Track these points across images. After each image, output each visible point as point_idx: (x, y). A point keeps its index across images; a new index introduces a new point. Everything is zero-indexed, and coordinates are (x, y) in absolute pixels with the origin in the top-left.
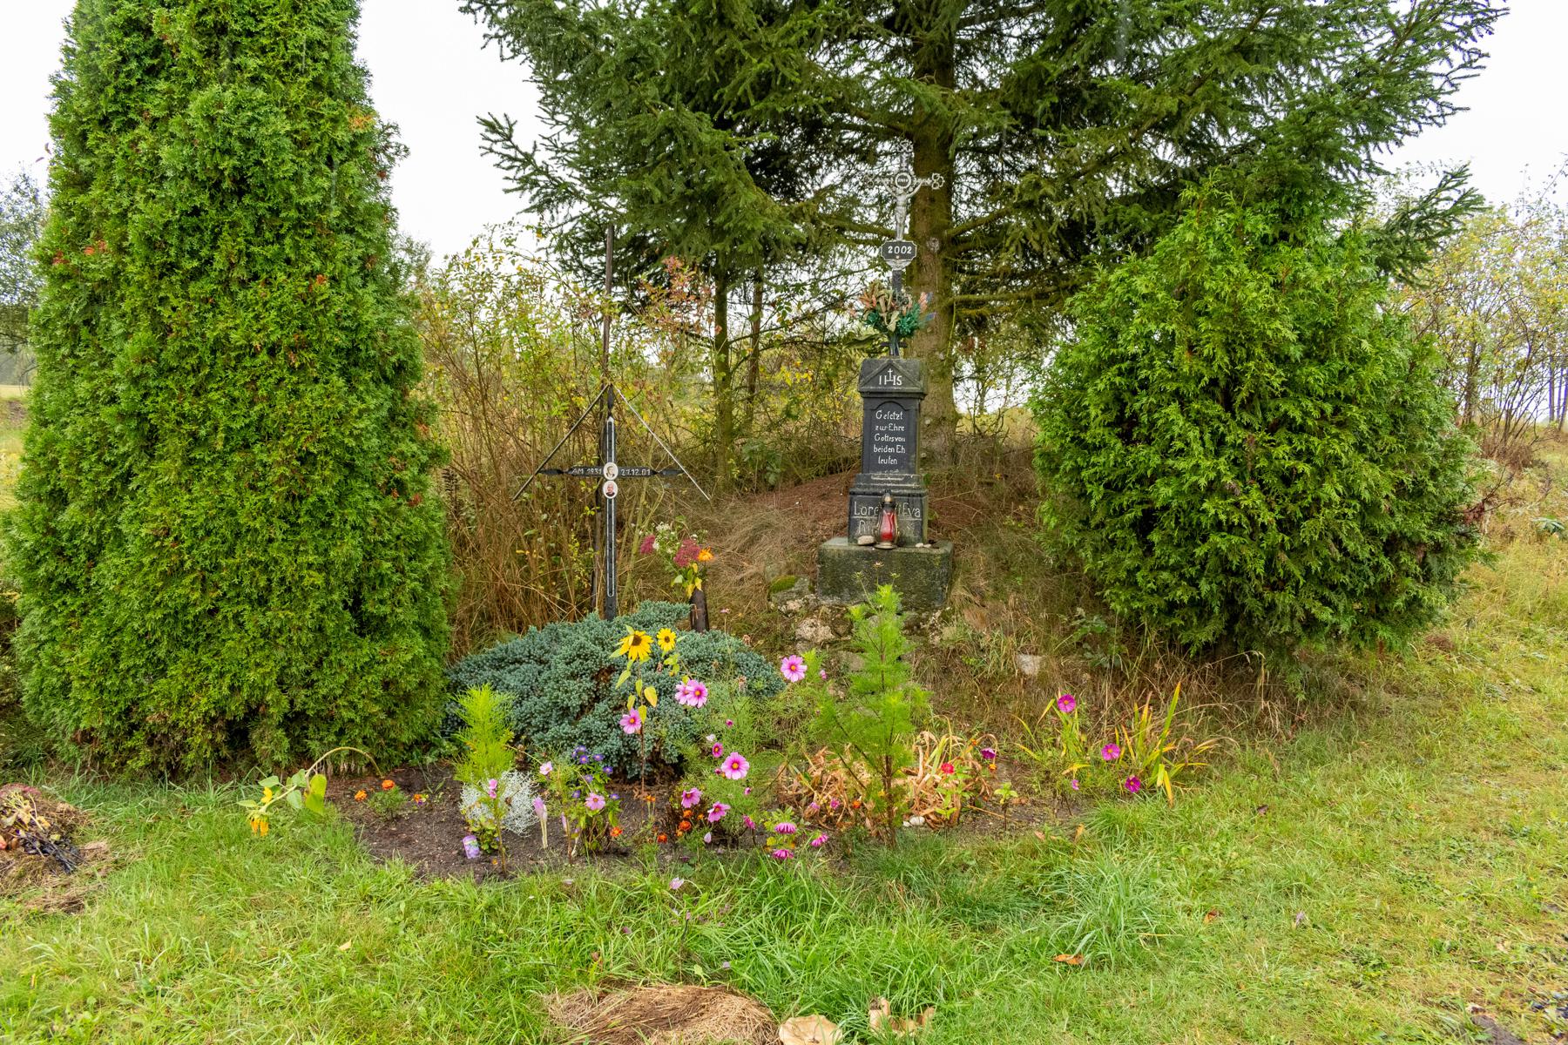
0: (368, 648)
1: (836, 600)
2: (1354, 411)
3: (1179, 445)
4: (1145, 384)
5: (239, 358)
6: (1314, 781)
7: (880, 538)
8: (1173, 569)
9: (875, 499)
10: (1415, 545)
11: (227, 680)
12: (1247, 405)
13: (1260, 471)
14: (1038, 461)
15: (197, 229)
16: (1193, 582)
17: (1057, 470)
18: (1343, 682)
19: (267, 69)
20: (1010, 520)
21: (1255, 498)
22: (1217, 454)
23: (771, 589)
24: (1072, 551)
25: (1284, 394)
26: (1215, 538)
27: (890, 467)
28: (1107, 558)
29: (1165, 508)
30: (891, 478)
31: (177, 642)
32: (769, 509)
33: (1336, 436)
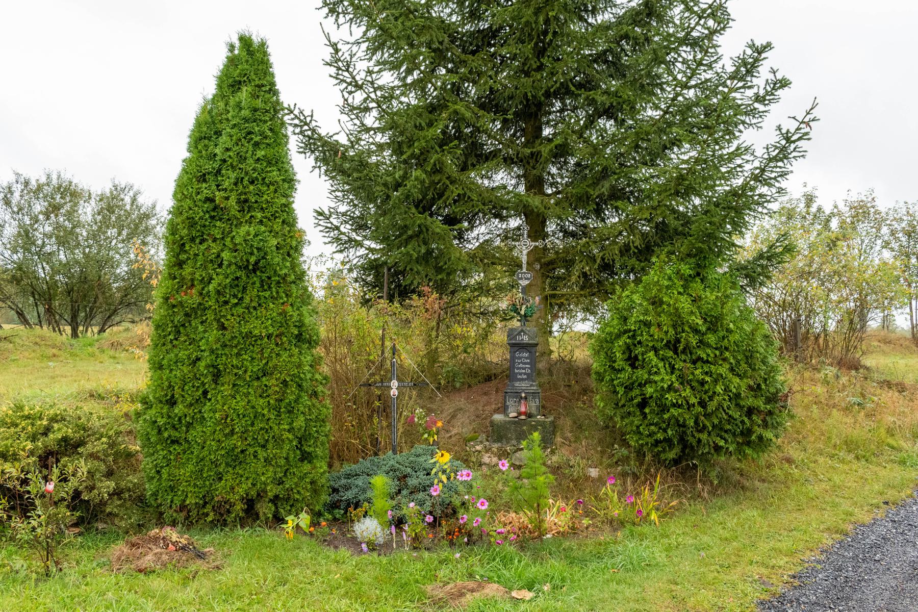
0: (306, 467)
1: (500, 444)
2: (727, 354)
3: (655, 370)
4: (640, 343)
5: (256, 341)
6: (719, 516)
7: (520, 414)
8: (656, 425)
9: (517, 395)
10: (760, 412)
11: (251, 481)
12: (684, 352)
13: (691, 380)
14: (594, 376)
15: (237, 286)
16: (665, 431)
17: (602, 380)
18: (738, 477)
19: (266, 217)
20: (580, 404)
21: (688, 392)
22: (672, 373)
23: (467, 441)
24: (611, 418)
25: (698, 347)
26: (672, 410)
27: (523, 380)
28: (627, 421)
29: (651, 397)
30: (524, 385)
31: (227, 465)
32: (460, 401)
33: (721, 365)
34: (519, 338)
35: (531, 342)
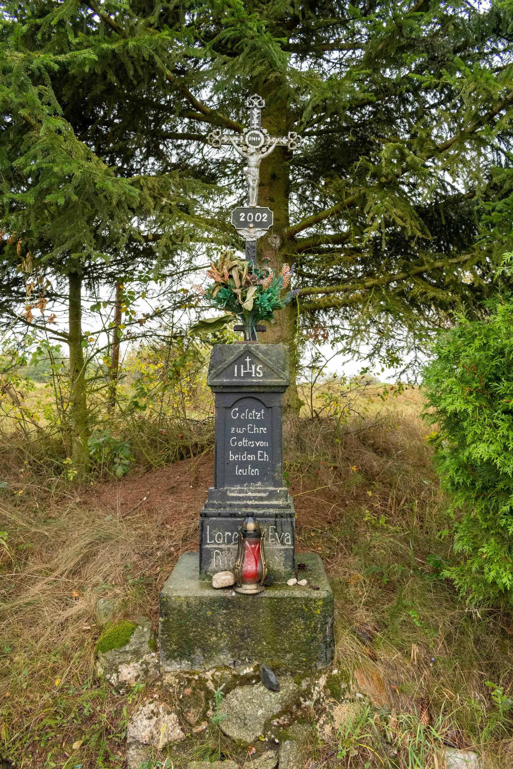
1: (185, 665)
27: (251, 479)
34: (239, 373)
35: (269, 381)
